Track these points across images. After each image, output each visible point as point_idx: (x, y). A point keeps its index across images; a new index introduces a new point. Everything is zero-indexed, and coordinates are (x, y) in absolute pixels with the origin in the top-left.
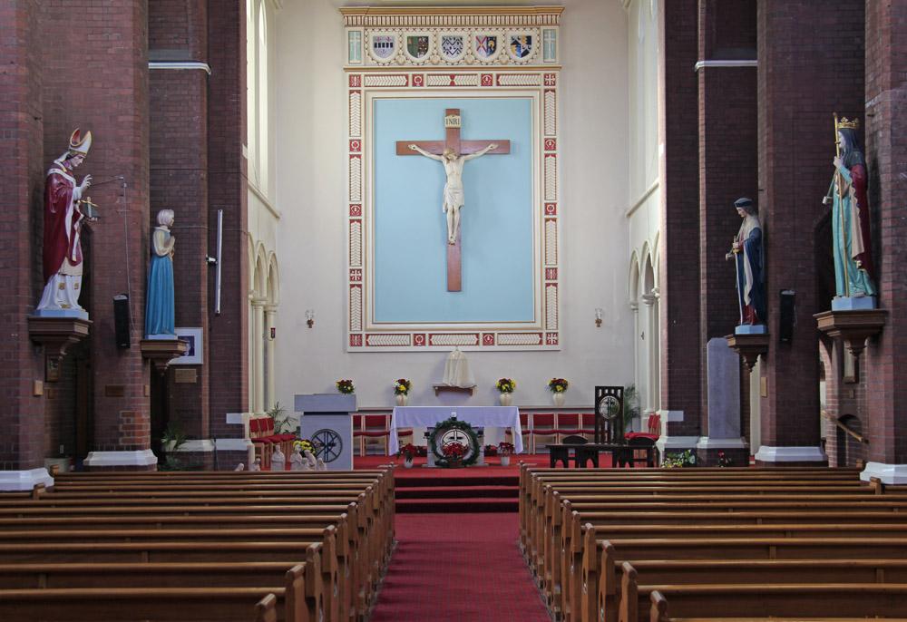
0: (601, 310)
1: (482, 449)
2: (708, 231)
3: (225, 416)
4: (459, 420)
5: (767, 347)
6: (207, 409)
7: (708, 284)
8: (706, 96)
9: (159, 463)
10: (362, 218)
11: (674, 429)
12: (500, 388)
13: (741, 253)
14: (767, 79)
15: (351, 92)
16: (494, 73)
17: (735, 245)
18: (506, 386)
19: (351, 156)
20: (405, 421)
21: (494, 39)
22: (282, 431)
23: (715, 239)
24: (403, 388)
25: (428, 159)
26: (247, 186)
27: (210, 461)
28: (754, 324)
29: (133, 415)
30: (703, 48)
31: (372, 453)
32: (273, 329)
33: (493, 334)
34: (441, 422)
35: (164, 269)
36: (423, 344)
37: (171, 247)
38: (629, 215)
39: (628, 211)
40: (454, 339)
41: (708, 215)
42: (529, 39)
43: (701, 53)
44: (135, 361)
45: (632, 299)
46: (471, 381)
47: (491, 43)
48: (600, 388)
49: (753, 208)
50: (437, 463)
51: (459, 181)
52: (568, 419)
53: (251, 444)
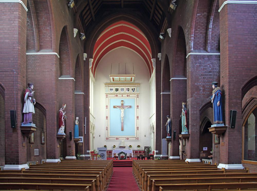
1: (127, 157)
11: (157, 154)
12: (130, 147)
13: (167, 125)
16: (129, 94)
17: (167, 123)
18: (130, 146)
21: (129, 89)
24: (114, 147)
25: (118, 109)
27: (84, 158)
29: (72, 150)
35: (77, 127)
37: (78, 123)
40: (122, 139)
42: (134, 89)
43: (162, 91)
45: (150, 132)
46: (125, 146)
47: (128, 89)
50: (120, 159)
52: (140, 152)
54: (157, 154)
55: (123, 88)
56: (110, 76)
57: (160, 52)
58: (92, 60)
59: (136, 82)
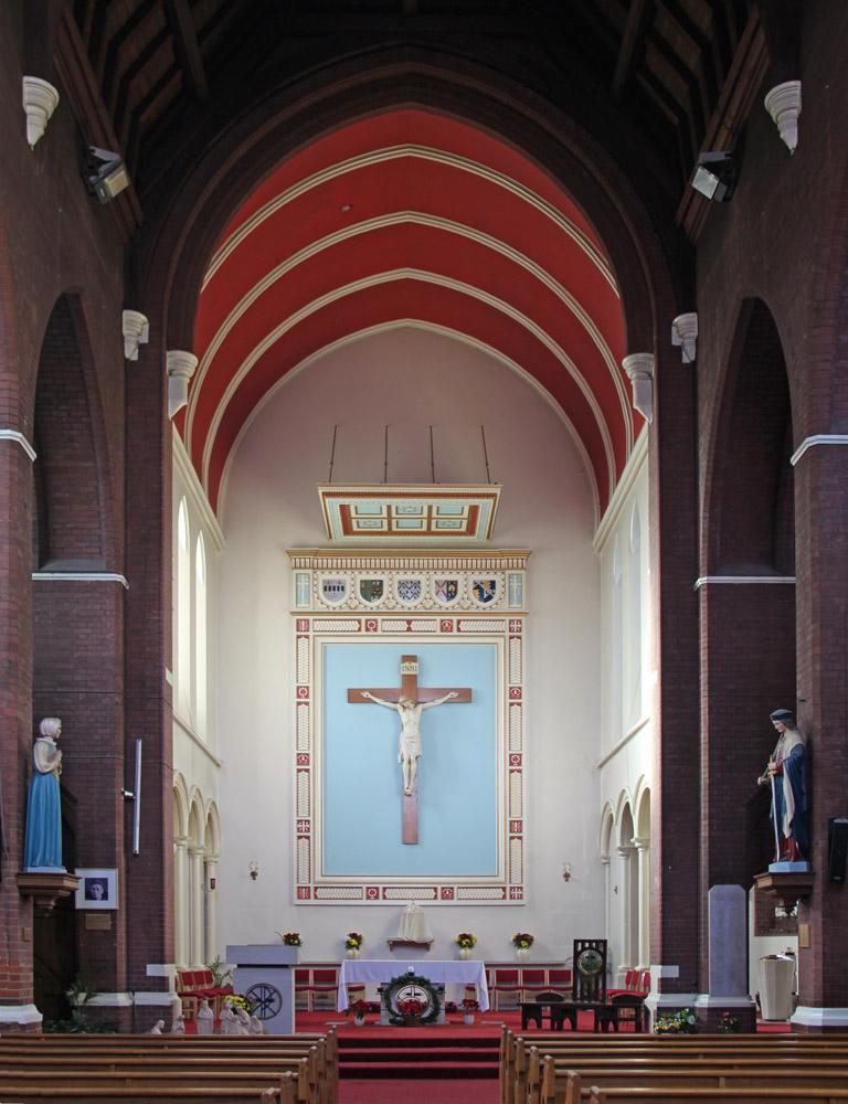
0: (570, 864)
1: (443, 1006)
2: (710, 767)
3: (145, 968)
4: (416, 975)
5: (811, 888)
6: (124, 959)
7: (710, 825)
8: (710, 615)
9: (43, 1022)
10: (310, 767)
11: (667, 986)
12: (460, 943)
13: (779, 774)
14: (813, 566)
15: (298, 637)
16: (455, 618)
17: (772, 765)
18: (465, 941)
19: (299, 704)
20: (354, 973)
21: (454, 583)
22: (224, 985)
23: (719, 775)
24: (354, 942)
25: (380, 710)
26: (172, 717)
27: (126, 1016)
28: (795, 861)
30: (706, 562)
31: (320, 1008)
32: (213, 880)
33: (452, 888)
34: (396, 977)
35: (47, 793)
36: (377, 897)
37: (57, 762)
38: (601, 766)
39: (600, 763)
40: (410, 893)
41: (711, 749)
42: (493, 584)
44: (9, 898)
45: (603, 853)
46: (428, 936)
47: (452, 588)
48: (579, 941)
49: (791, 720)
50: (391, 1021)
51: (417, 731)
52: (533, 976)
53: (177, 998)
54: (667, 986)
55: (416, 577)
56: (326, 494)
57: (689, 307)
58: (185, 368)
59: (504, 540)
